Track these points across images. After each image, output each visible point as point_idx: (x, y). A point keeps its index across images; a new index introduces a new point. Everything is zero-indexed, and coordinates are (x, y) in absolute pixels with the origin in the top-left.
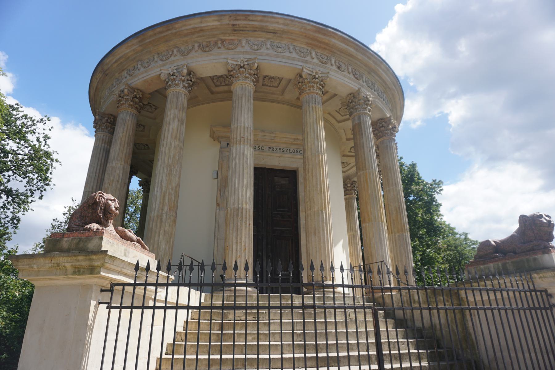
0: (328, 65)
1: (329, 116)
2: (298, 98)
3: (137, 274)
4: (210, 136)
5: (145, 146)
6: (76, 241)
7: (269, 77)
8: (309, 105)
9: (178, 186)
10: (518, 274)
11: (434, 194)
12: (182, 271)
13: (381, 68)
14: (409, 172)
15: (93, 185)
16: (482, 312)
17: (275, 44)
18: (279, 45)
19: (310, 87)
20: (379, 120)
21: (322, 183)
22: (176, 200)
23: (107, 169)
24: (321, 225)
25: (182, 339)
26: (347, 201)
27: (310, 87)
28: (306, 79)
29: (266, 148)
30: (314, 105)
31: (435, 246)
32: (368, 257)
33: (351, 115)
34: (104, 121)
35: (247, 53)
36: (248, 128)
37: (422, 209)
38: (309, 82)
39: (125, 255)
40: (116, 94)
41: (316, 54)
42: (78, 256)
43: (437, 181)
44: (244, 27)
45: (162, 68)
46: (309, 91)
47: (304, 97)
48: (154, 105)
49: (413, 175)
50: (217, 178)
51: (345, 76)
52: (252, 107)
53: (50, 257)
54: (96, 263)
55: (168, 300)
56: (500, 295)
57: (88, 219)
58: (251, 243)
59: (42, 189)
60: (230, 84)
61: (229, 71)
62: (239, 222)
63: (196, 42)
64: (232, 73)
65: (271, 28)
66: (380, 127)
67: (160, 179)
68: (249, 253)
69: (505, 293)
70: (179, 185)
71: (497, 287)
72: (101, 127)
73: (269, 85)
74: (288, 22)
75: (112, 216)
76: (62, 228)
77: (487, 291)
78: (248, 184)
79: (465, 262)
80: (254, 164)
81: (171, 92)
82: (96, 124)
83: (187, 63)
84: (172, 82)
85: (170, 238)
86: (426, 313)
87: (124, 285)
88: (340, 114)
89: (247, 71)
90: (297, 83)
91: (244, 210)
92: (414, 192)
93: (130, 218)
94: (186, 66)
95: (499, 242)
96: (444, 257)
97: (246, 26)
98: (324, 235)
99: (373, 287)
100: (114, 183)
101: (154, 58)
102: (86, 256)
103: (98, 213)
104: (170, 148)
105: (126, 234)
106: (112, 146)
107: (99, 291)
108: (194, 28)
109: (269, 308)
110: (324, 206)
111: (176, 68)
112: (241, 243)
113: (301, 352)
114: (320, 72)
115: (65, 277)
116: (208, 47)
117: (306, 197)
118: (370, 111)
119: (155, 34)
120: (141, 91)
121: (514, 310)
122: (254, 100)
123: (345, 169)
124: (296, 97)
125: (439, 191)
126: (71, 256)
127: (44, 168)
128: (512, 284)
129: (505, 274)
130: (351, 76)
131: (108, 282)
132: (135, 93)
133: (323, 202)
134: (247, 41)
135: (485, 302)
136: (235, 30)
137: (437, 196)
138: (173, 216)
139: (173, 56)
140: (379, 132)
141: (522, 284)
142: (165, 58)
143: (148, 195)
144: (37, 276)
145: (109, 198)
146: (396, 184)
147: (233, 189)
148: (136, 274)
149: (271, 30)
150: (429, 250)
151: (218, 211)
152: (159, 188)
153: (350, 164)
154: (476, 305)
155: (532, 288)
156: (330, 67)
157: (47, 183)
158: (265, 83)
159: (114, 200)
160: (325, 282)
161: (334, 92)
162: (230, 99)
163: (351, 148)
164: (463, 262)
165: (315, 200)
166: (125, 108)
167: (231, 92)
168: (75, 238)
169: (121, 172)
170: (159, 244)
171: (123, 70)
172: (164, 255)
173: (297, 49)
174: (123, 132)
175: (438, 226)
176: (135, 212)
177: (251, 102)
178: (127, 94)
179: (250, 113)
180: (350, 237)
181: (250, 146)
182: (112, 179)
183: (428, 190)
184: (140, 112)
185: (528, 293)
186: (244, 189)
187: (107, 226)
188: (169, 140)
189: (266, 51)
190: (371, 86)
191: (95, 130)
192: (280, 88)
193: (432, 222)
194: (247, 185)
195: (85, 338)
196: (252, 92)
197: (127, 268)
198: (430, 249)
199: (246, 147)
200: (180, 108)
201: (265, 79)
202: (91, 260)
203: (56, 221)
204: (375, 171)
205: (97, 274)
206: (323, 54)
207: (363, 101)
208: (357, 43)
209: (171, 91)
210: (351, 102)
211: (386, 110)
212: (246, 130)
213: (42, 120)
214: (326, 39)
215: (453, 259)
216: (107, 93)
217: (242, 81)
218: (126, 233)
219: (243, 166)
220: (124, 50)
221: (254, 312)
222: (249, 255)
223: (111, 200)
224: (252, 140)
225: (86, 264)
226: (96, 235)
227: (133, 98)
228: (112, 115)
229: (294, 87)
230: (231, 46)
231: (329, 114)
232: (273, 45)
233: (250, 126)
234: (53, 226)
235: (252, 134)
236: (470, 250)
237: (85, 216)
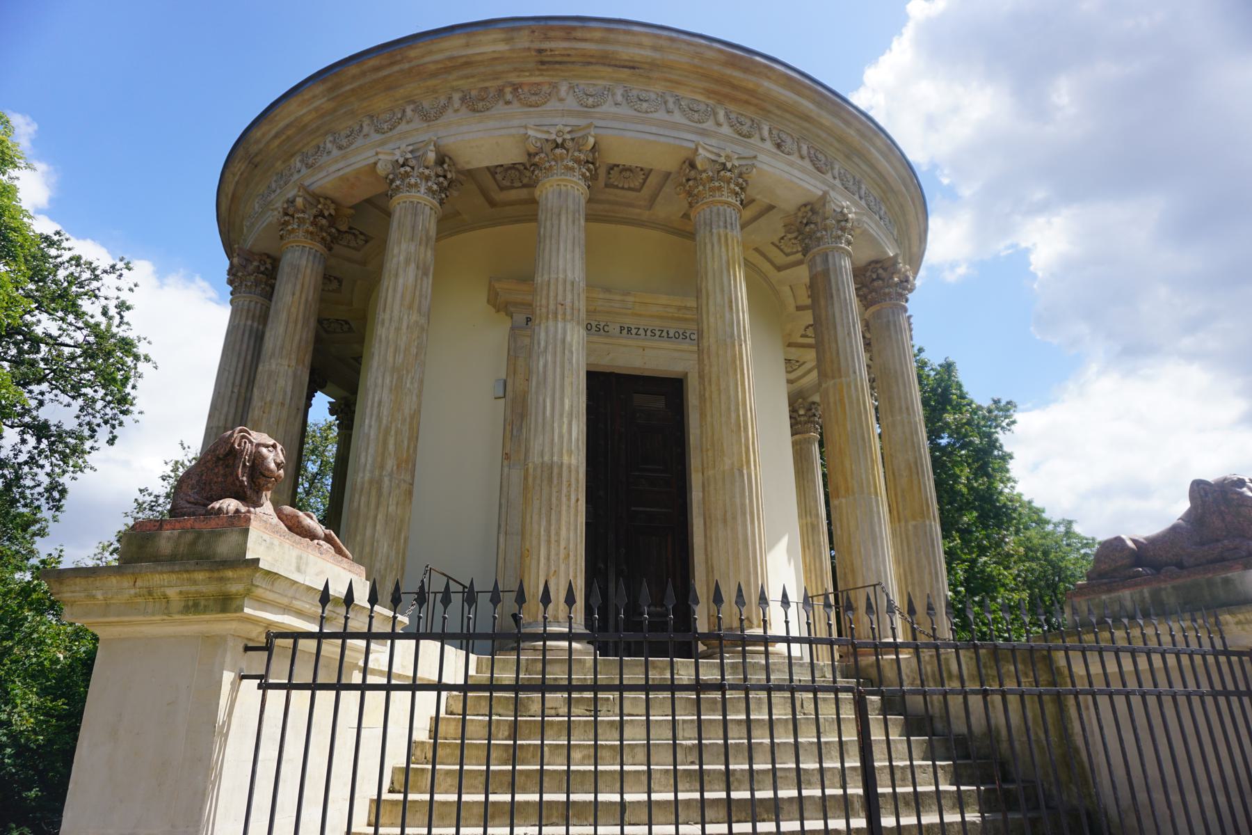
0: (755, 140)
1: (756, 255)
2: (686, 216)
3: (326, 612)
4: (488, 302)
5: (342, 325)
6: (189, 537)
7: (621, 167)
9: (416, 414)
10: (1187, 616)
11: (996, 432)
13: (873, 145)
14: (939, 382)
15: (228, 412)
16: (1103, 701)
17: (635, 92)
18: (643, 95)
19: (712, 189)
20: (870, 263)
21: (740, 407)
22: (412, 446)
23: (258, 377)
24: (738, 501)
25: (426, 758)
26: (798, 447)
27: (712, 189)
28: (705, 171)
29: (614, 329)
30: (722, 231)
31: (998, 550)
32: (845, 574)
33: (807, 253)
34: (251, 268)
35: (571, 113)
36: (573, 283)
37: (969, 465)
38: (711, 179)
39: (299, 570)
40: (276, 209)
41: (727, 115)
42: (194, 571)
43: (1003, 403)
44: (563, 55)
45: (378, 150)
47: (699, 213)
48: (361, 233)
49: (946, 390)
50: (505, 397)
51: (791, 164)
52: (583, 236)
53: (133, 574)
54: (234, 588)
55: (394, 670)
56: (1147, 663)
57: (215, 488)
58: (582, 541)
59: (114, 422)
60: (532, 185)
61: (530, 155)
62: (554, 494)
63: (455, 89)
64: (537, 159)
66: (873, 280)
67: (376, 399)
68: (576, 564)
71: (1138, 643)
72: (244, 283)
73: (620, 185)
74: (662, 42)
75: (270, 482)
76: (159, 509)
77: (1117, 652)
78: (574, 410)
79: (1066, 587)
80: (587, 364)
81: (399, 203)
82: (233, 275)
83: (435, 138)
84: (403, 181)
85: (400, 531)
86: (975, 702)
87: (297, 636)
88: (782, 250)
89: (570, 154)
90: (684, 180)
91: (565, 468)
92: (950, 428)
94: (432, 144)
95: (1145, 542)
96: (1019, 575)
97: (569, 52)
98: (746, 525)
99: (856, 641)
100: (274, 407)
101: (361, 126)
102: (212, 571)
103: (237, 475)
104: (398, 329)
105: (299, 522)
106: (269, 326)
107: (241, 649)
108: (451, 58)
109: (622, 688)
110: (744, 459)
111: (411, 148)
112: (558, 542)
113: (693, 788)
114: (736, 157)
115: (165, 617)
116: (483, 100)
117: (704, 439)
118: (849, 243)
119: (364, 74)
120: (333, 202)
121: (1178, 697)
122: (587, 220)
123: (793, 376)
124: (682, 213)
125: (1008, 425)
127: (119, 376)
128: (1173, 636)
129: (1157, 615)
130: (807, 164)
131: (260, 629)
132: (320, 206)
134: (571, 88)
135: (1110, 678)
136: (543, 63)
137: (1001, 437)
140: (871, 292)
141: (1197, 636)
142: (386, 127)
143: (350, 436)
144: (105, 616)
145: (262, 442)
146: (909, 410)
147: (540, 420)
148: (323, 612)
149: (626, 60)
150: (985, 559)
151: (506, 470)
152: (374, 418)
153: (804, 363)
154: (1091, 684)
155: (1219, 646)
156: (760, 144)
158: (612, 180)
159: (274, 446)
160: (748, 632)
162: (533, 218)
163: (807, 327)
164: (1061, 586)
165: (725, 445)
166: (296, 239)
167: (534, 201)
169: (290, 383)
170: (375, 544)
171: (292, 156)
172: (386, 569)
173: (682, 103)
174: (294, 294)
175: (1005, 505)
176: (321, 473)
177: (579, 224)
178: (302, 208)
179: (577, 250)
180: (805, 529)
181: (578, 323)
182: (268, 399)
183: (982, 423)
184: (330, 249)
185: (1210, 659)
186: (565, 420)
187: (257, 504)
188: (396, 313)
189: (614, 109)
190: (851, 186)
191: (231, 289)
192: (646, 192)
193: (992, 495)
194: (572, 410)
195: (211, 755)
196: (583, 202)
197: (304, 599)
198: (987, 556)
199: (569, 326)
200: (421, 239)
201: (611, 172)
202: (221, 579)
203: (146, 493)
205: (236, 611)
206: (742, 115)
207: (834, 222)
209: (401, 201)
210: (807, 224)
211: (885, 239)
212: (569, 287)
213: (113, 267)
214: (750, 81)
215: (1038, 579)
216: (257, 206)
218: (301, 519)
219: (563, 368)
220: (294, 110)
221: (587, 698)
222: (576, 569)
223: (267, 446)
224: (583, 309)
225: (211, 589)
226: (232, 525)
227: (315, 217)
228: (269, 256)
229: (678, 189)
230: (534, 98)
231: (756, 250)
232: (630, 94)
233: (577, 279)
234: (140, 505)
235: (583, 297)
236: (1077, 559)
237: (210, 484)
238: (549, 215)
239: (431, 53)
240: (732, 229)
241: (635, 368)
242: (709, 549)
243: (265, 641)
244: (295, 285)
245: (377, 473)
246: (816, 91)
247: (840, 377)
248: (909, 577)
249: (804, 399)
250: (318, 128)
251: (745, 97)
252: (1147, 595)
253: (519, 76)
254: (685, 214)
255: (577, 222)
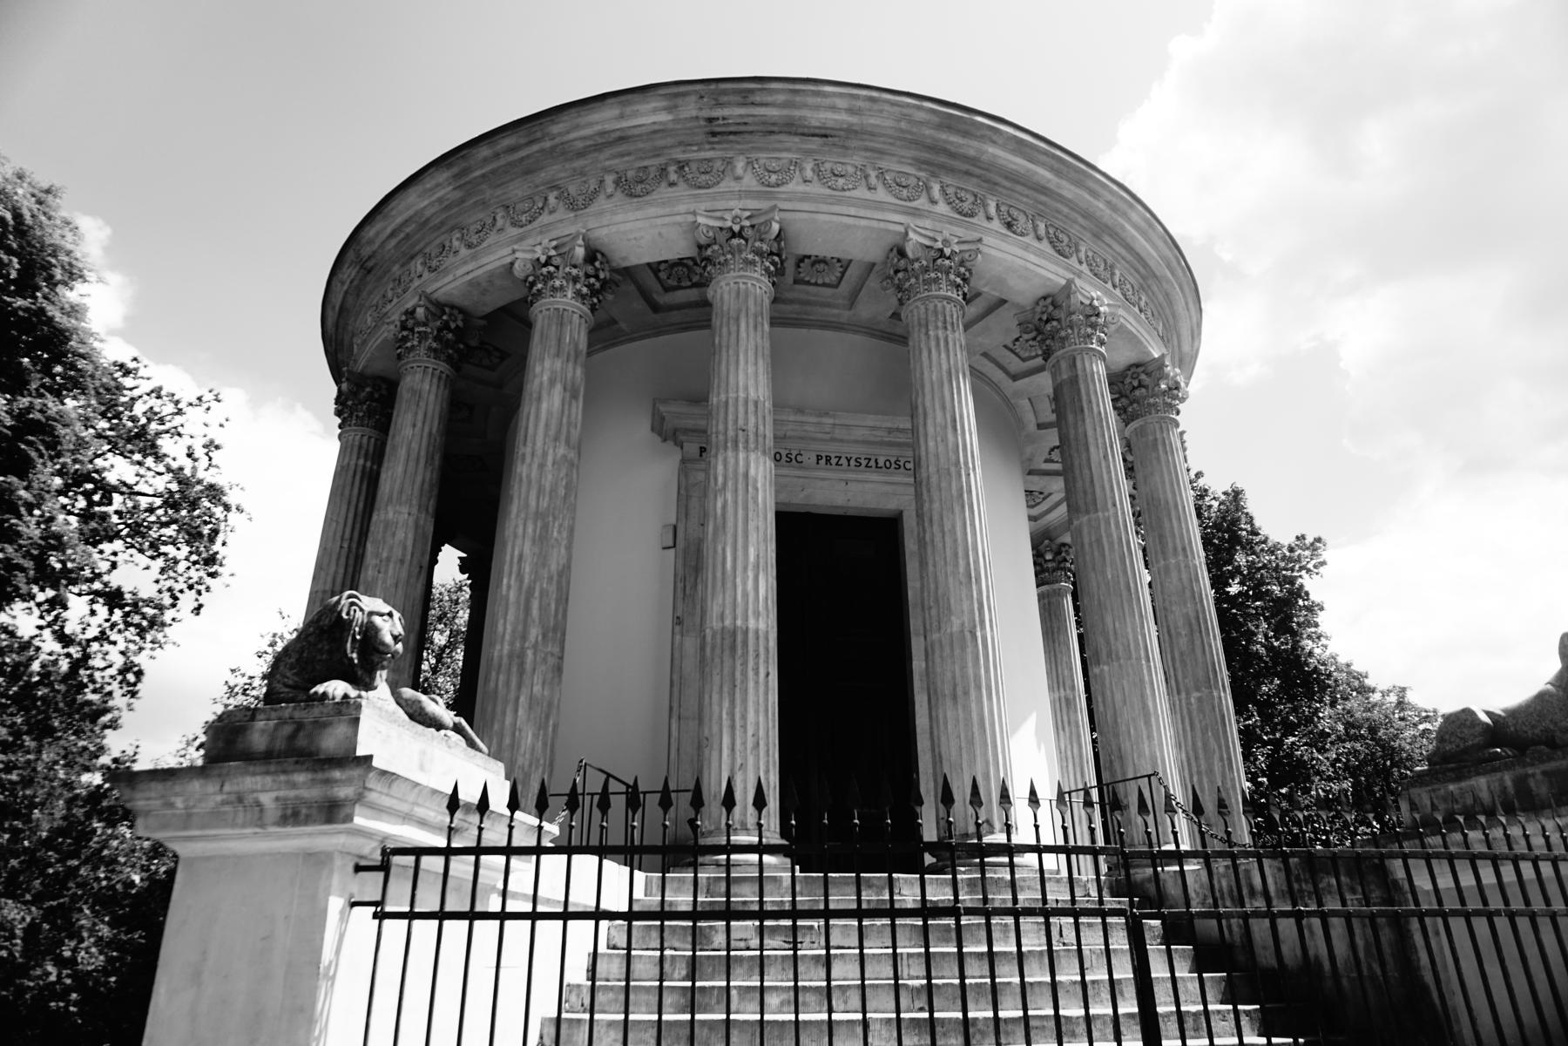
0: (979, 220)
1: (985, 361)
2: (896, 316)
4: (653, 429)
6: (288, 729)
8: (927, 334)
9: (565, 572)
12: (641, 809)
13: (1129, 220)
14: (1223, 515)
17: (828, 166)
20: (1129, 367)
24: (971, 671)
27: (927, 282)
28: (917, 260)
30: (940, 333)
32: (1111, 762)
35: (749, 194)
36: (756, 403)
37: (1266, 619)
38: (926, 270)
40: (393, 322)
41: (943, 190)
42: (293, 772)
43: (1309, 540)
45: (516, 247)
46: (926, 294)
48: (497, 349)
51: (1026, 248)
52: (767, 345)
53: (219, 775)
54: (343, 792)
56: (1513, 873)
57: (318, 667)
59: (199, 587)
60: (703, 284)
61: (700, 247)
63: (607, 170)
64: (709, 252)
65: (815, 123)
66: (1134, 388)
67: (516, 553)
68: (768, 755)
69: (1527, 869)
70: (569, 567)
74: (860, 104)
80: (776, 503)
81: (541, 311)
82: (341, 404)
85: (547, 717)
86: (1287, 926)
87: (419, 852)
90: (892, 272)
91: (751, 635)
92: (1241, 573)
93: (438, 662)
96: (1337, 760)
99: (1127, 850)
101: (494, 219)
102: (315, 771)
104: (542, 466)
105: (422, 708)
106: (385, 465)
107: (350, 868)
108: (602, 133)
110: (977, 619)
111: (554, 243)
112: (744, 727)
115: (258, 830)
116: (642, 182)
118: (1102, 343)
119: (497, 156)
122: (772, 324)
123: (1036, 511)
125: (1315, 567)
126: (275, 773)
127: (206, 530)
128: (1547, 838)
129: (1524, 810)
130: (1045, 246)
131: (374, 844)
132: (445, 317)
133: (976, 606)
134: (749, 163)
135: (1466, 894)
136: (714, 134)
137: (1307, 582)
138: (552, 654)
139: (546, 210)
140: (1131, 404)
142: (524, 219)
144: (185, 828)
145: (376, 610)
146: (1186, 550)
150: (1292, 739)
151: (678, 637)
153: (1050, 494)
154: (1440, 902)
156: (985, 224)
157: (212, 570)
159: (390, 615)
161: (997, 294)
162: (705, 323)
163: (1052, 450)
167: (706, 304)
168: (285, 723)
169: (411, 536)
171: (412, 258)
172: (530, 766)
174: (414, 426)
179: (761, 362)
181: (764, 453)
182: (385, 555)
186: (751, 574)
187: (369, 687)
188: (539, 444)
189: (802, 188)
190: (1103, 272)
191: (339, 421)
192: (845, 287)
196: (767, 302)
198: (1295, 736)
199: (752, 456)
204: (1123, 513)
205: (344, 822)
208: (1059, 153)
210: (1047, 321)
212: (751, 408)
213: (200, 399)
214: (971, 147)
215: (1364, 763)
216: (369, 319)
217: (737, 274)
219: (746, 509)
220: (415, 202)
224: (769, 434)
225: (314, 793)
226: (340, 713)
230: (703, 177)
231: (985, 355)
234: (231, 689)
235: (769, 420)
238: (725, 320)
239: (577, 127)
240: (954, 331)
241: (837, 507)
242: (935, 733)
243: (380, 858)
244: (416, 414)
245: (518, 645)
246: (1054, 157)
247: (1096, 511)
248: (1194, 764)
249: (1051, 540)
250: (443, 223)
251: (965, 167)
252: (1509, 783)
253: (684, 152)
254: (894, 314)
255: (759, 328)
